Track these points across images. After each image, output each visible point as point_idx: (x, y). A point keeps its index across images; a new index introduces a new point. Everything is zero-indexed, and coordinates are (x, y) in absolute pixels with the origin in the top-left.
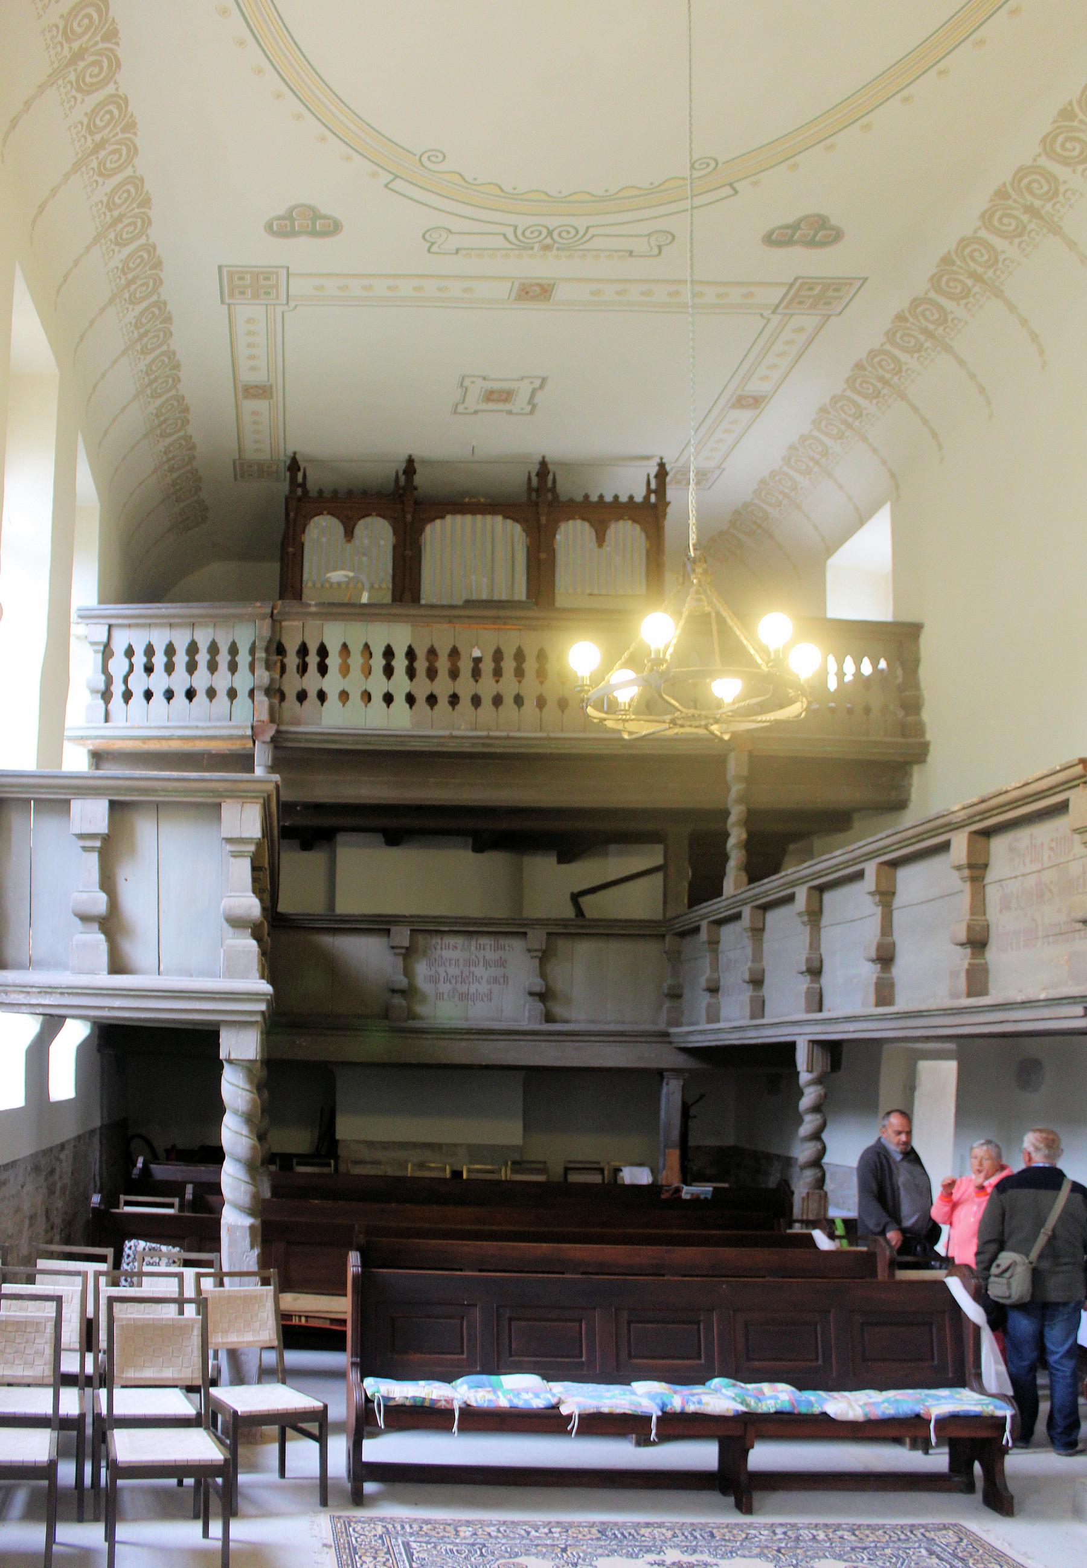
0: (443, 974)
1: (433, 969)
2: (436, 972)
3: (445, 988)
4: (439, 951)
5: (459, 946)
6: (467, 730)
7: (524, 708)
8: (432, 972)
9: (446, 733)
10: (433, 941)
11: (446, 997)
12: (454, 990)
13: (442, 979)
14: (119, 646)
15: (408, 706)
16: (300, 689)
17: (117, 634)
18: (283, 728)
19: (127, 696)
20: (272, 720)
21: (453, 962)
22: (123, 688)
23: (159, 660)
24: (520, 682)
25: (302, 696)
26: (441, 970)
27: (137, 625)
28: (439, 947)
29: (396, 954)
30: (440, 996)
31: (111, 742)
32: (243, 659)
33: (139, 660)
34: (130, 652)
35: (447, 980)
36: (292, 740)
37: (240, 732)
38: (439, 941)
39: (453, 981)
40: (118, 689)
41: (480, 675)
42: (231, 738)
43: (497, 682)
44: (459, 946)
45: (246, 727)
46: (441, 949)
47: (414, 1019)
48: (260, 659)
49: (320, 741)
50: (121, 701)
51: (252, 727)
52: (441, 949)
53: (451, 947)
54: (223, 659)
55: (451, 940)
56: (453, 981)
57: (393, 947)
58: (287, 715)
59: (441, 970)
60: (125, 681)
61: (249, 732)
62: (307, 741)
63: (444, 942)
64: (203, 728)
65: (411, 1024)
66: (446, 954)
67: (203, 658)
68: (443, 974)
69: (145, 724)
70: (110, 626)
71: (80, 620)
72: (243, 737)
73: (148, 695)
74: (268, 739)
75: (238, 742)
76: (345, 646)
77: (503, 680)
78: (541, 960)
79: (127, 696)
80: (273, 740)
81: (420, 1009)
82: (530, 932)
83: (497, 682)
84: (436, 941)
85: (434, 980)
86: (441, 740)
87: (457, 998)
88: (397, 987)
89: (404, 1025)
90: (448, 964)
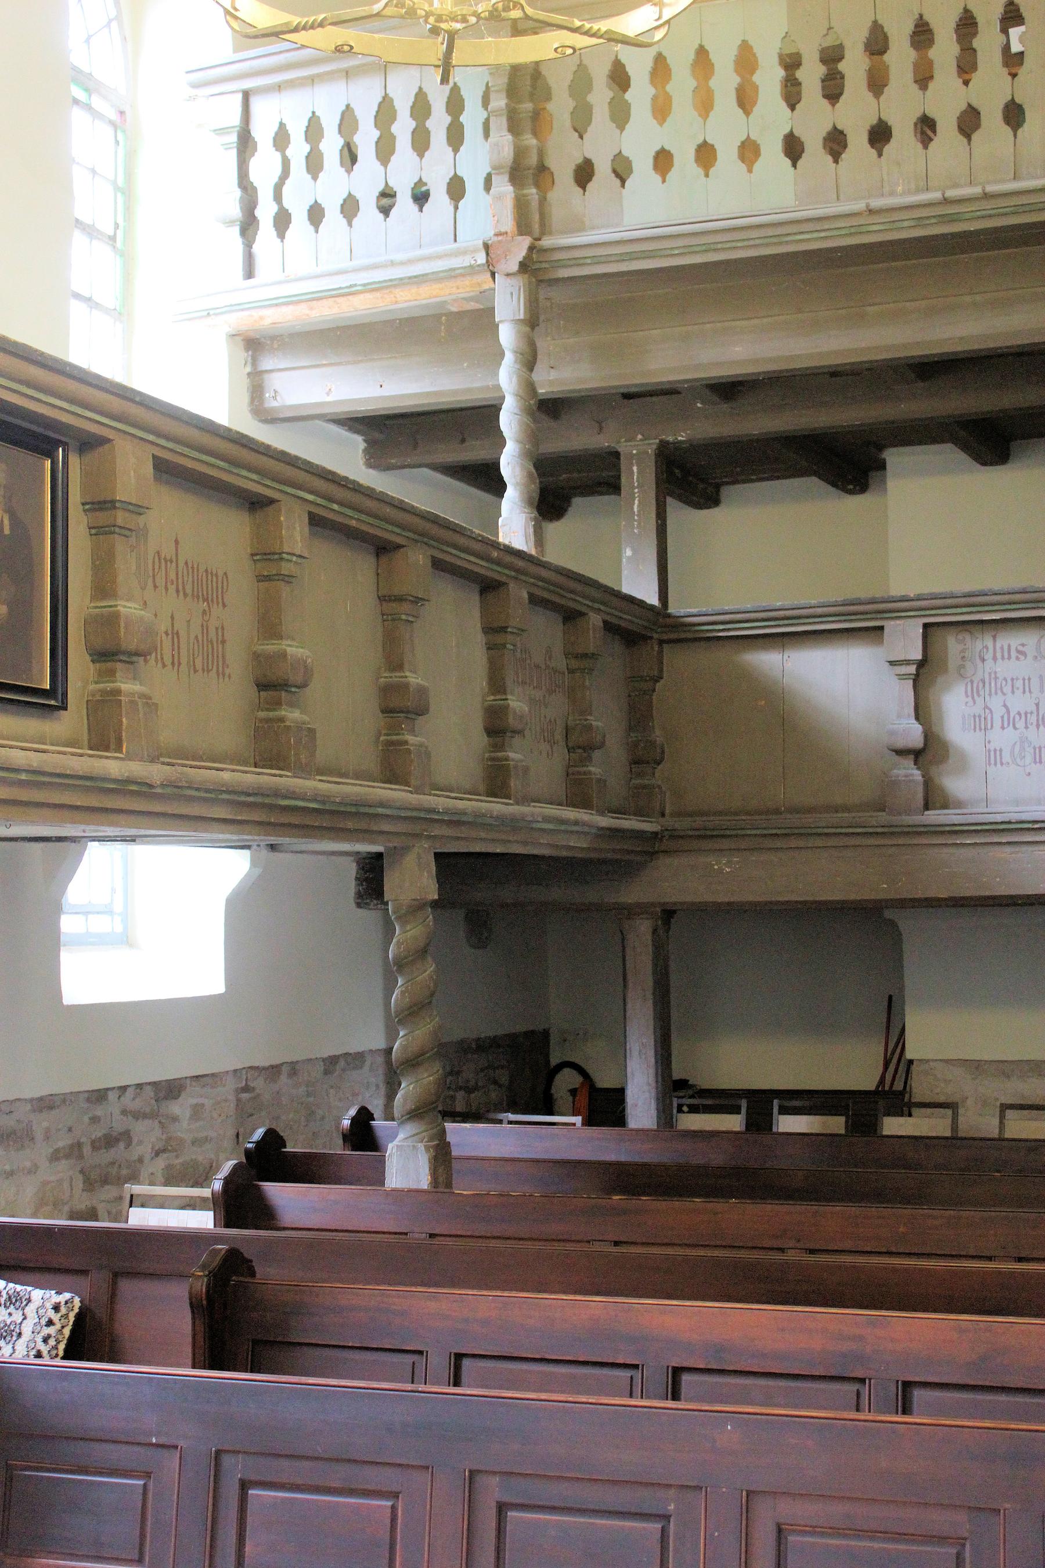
0: (999, 711)
1: (980, 701)
2: (986, 707)
3: (1002, 738)
4: (989, 662)
5: (1030, 650)
6: (907, 192)
7: (1023, 132)
8: (978, 710)
9: (860, 206)
10: (979, 645)
11: (1006, 757)
12: (1023, 740)
13: (997, 723)
14: (263, 132)
15: (788, 162)
16: (580, 160)
17: (258, 105)
18: (546, 242)
19: (282, 221)
20: (523, 226)
21: (1019, 684)
22: (274, 208)
23: (366, 139)
24: (1014, 76)
25: (584, 174)
26: (996, 703)
27: (291, 84)
28: (989, 656)
29: (902, 677)
30: (994, 757)
31: (256, 314)
32: (472, 117)
33: (298, 149)
34: (281, 139)
35: (1009, 721)
36: (578, 262)
37: (466, 261)
38: (989, 643)
39: (1020, 724)
40: (266, 211)
41: (974, 67)
42: (451, 275)
43: (966, 83)
44: (1030, 650)
45: (475, 251)
46: (995, 659)
47: (945, 806)
48: (497, 113)
49: (622, 258)
50: (273, 233)
51: (487, 247)
52: (995, 659)
53: (1014, 654)
54: (438, 122)
55: (1012, 640)
56: (1020, 724)
57: (892, 663)
58: (557, 214)
59: (996, 703)
60: (278, 196)
61: (481, 258)
62: (597, 261)
63: (998, 645)
64: (402, 263)
65: (934, 817)
66: (1005, 669)
67: (403, 127)
68: (999, 711)
69: (347, 264)
70: (246, 95)
71: (194, 92)
72: (472, 270)
73: (316, 214)
74: (514, 267)
75: (467, 281)
76: (702, 52)
77: (976, 78)
78: (916, 680)
79: (282, 221)
80: (524, 267)
81: (955, 785)
82: (889, 625)
83: (966, 83)
84: (984, 643)
85: (982, 723)
86: (855, 222)
87: (1029, 759)
88: (901, 744)
89: (918, 819)
90: (1007, 689)
